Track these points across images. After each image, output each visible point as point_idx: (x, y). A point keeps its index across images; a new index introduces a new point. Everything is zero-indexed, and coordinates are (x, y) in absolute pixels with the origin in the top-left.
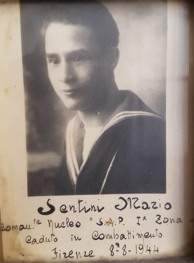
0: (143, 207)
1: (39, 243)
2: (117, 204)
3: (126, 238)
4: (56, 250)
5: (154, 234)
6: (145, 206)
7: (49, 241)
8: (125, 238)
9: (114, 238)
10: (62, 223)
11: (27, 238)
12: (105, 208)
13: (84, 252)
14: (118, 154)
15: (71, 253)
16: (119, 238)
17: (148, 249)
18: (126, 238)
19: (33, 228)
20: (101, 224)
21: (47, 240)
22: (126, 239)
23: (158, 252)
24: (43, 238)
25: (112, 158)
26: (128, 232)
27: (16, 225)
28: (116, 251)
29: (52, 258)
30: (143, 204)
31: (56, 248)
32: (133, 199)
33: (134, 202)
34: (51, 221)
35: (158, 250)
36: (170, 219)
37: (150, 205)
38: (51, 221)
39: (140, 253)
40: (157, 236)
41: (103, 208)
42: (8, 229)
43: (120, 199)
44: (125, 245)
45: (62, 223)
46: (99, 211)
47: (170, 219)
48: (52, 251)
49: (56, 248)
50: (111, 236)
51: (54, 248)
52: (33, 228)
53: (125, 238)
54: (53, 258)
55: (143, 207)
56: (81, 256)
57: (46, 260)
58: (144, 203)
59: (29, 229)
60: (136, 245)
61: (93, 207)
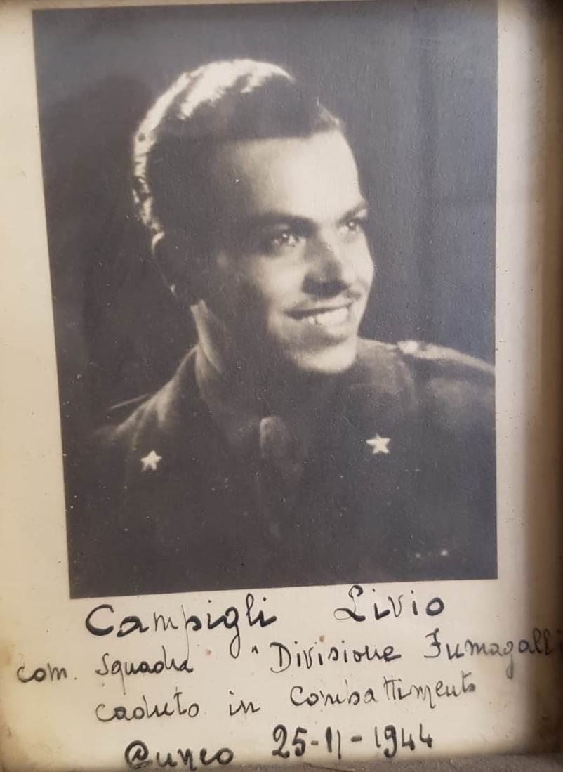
1: (162, 714)
4: (438, 635)
7: (165, 712)
9: (152, 626)
10: (235, 638)
13: (466, 645)
23: (433, 743)
24: (163, 661)
25: (116, 409)
27: (480, 654)
28: (179, 629)
29: (509, 680)
31: (437, 630)
34: (161, 618)
35: (438, 641)
38: (161, 618)
39: (107, 654)
41: (399, 656)
42: (495, 651)
44: (309, 668)
45: (235, 638)
46: (264, 624)
48: (427, 636)
49: (437, 630)
51: (433, 631)
52: (374, 590)
53: (144, 627)
54: (511, 677)
57: (217, 92)
59: (165, 669)
61: (53, 672)
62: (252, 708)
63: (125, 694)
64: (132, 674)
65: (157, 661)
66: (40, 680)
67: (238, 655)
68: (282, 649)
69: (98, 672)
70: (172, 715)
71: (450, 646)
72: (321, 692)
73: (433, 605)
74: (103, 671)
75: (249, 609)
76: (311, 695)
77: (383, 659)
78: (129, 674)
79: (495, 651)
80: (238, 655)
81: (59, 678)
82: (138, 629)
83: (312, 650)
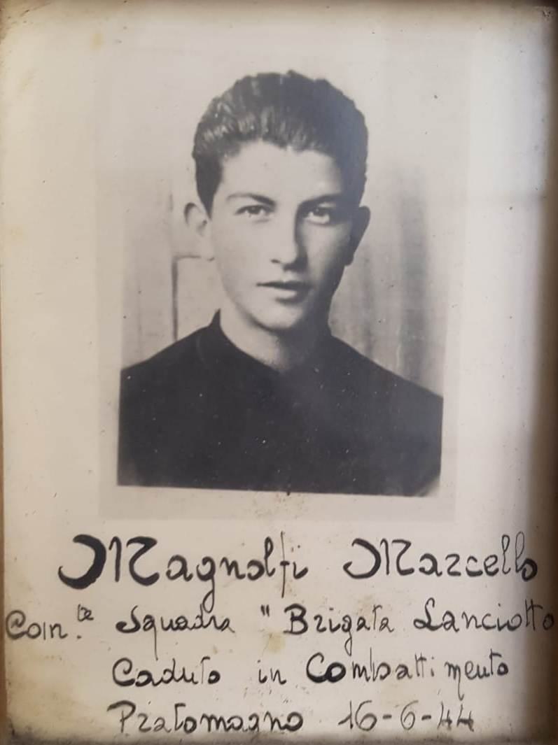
0: (422, 570)
1: (475, 677)
2: (347, 562)
3: (393, 630)
5: (285, 629)
6: (428, 565)
7: (192, 679)
8: (457, 628)
10: (507, 548)
11: (359, 713)
12: (114, 626)
14: (254, 84)
15: (506, 540)
16: (394, 675)
17: (465, 716)
18: (393, 630)
19: (299, 547)
20: (135, 628)
21: (482, 673)
22: (459, 632)
26: (233, 629)
30: (422, 559)
32: (395, 541)
33: (400, 551)
36: (45, 638)
37: (443, 566)
40: (374, 628)
42: (36, 633)
43: (356, 545)
45: (507, 548)
47: (45, 638)
50: (468, 624)
52: (299, 547)
55: (422, 570)
56: (63, 634)
58: (427, 556)
60: (369, 699)
62: (279, 679)
63: (157, 659)
64: (170, 630)
65: (337, 684)
66: (334, 680)
67: (314, 656)
68: (359, 722)
69: (120, 626)
70: (423, 554)
71: (164, 619)
72: (117, 579)
73: (364, 721)
74: (131, 625)
75: (505, 551)
76: (165, 672)
77: (482, 628)
78: (166, 629)
79: (470, 717)
80: (314, 656)
81: (360, 675)
82: (151, 683)
83: (369, 704)
